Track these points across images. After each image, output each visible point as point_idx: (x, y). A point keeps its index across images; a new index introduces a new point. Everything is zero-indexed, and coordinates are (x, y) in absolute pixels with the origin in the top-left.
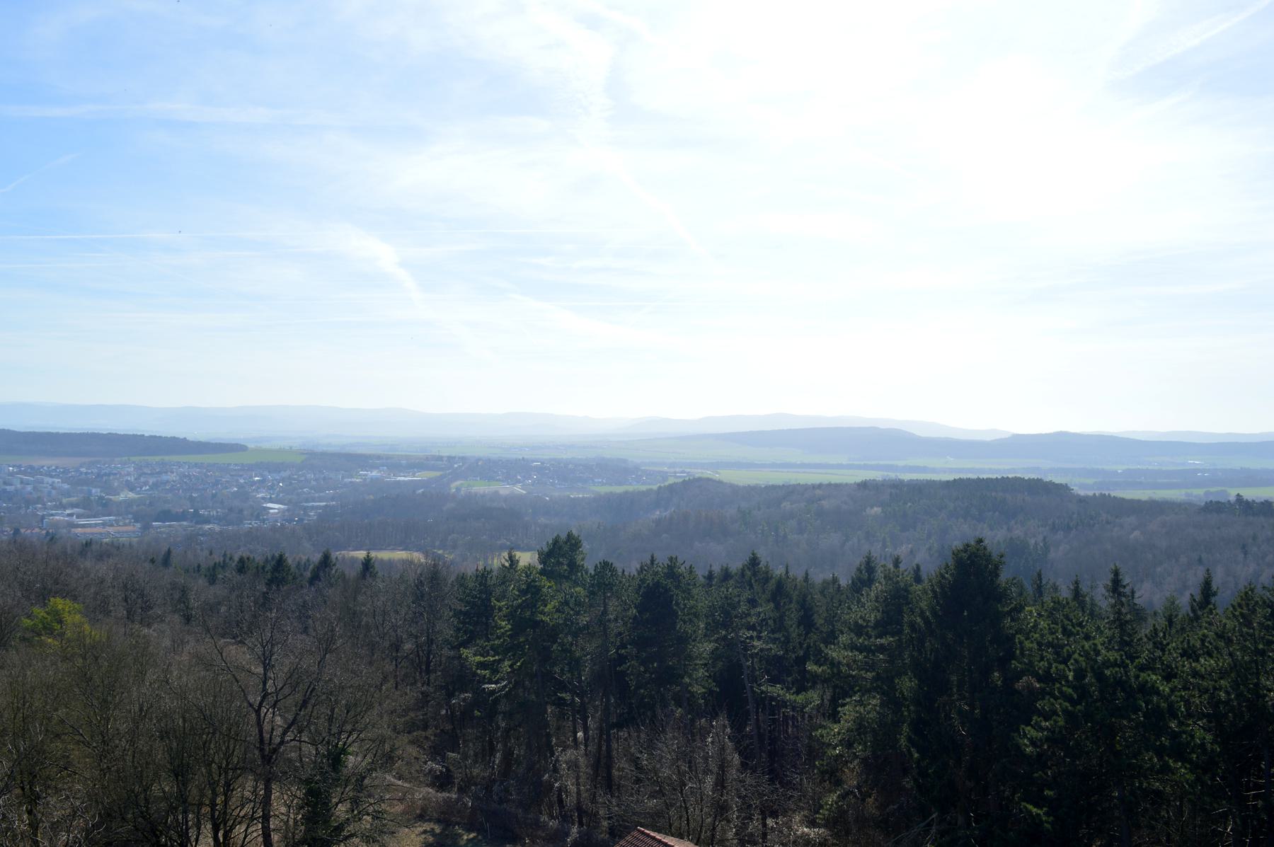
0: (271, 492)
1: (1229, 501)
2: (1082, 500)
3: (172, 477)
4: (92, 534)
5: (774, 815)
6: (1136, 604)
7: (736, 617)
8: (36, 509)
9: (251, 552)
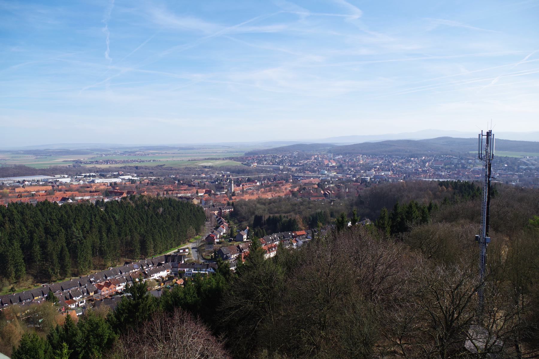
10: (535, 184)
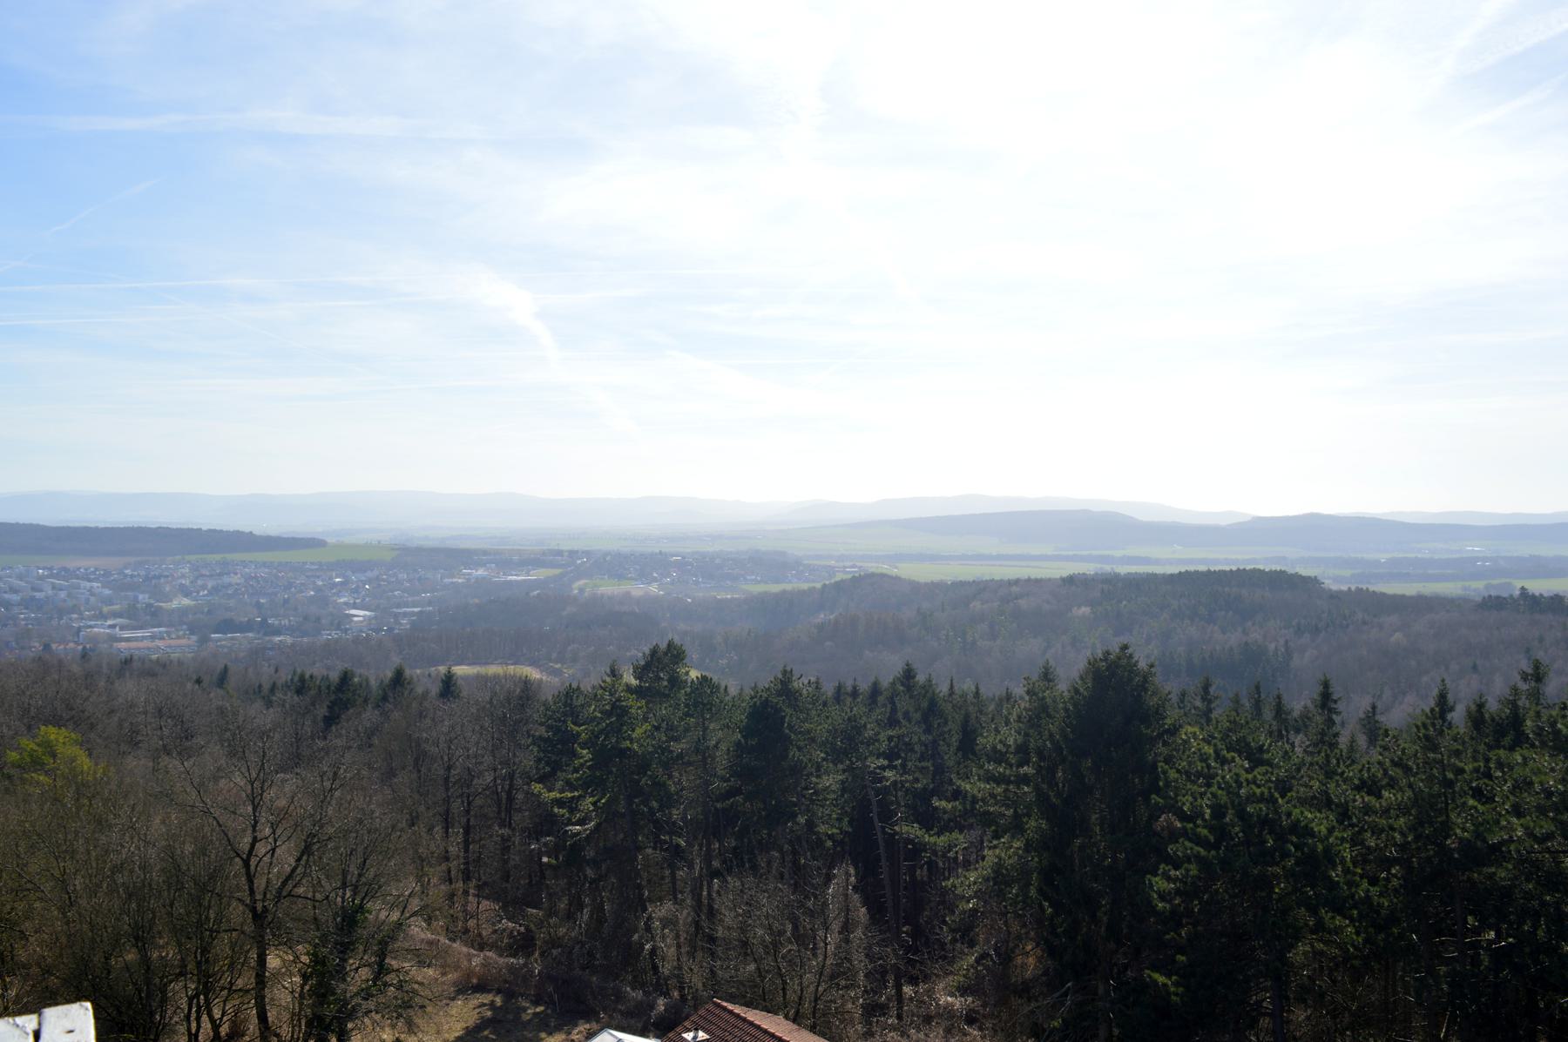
0: (356, 595)
1: (1511, 596)
2: (1335, 596)
3: (236, 579)
4: (139, 649)
5: (914, 981)
6: (1377, 722)
7: (862, 743)
8: (70, 619)
9: (328, 669)
10: (23, 648)
